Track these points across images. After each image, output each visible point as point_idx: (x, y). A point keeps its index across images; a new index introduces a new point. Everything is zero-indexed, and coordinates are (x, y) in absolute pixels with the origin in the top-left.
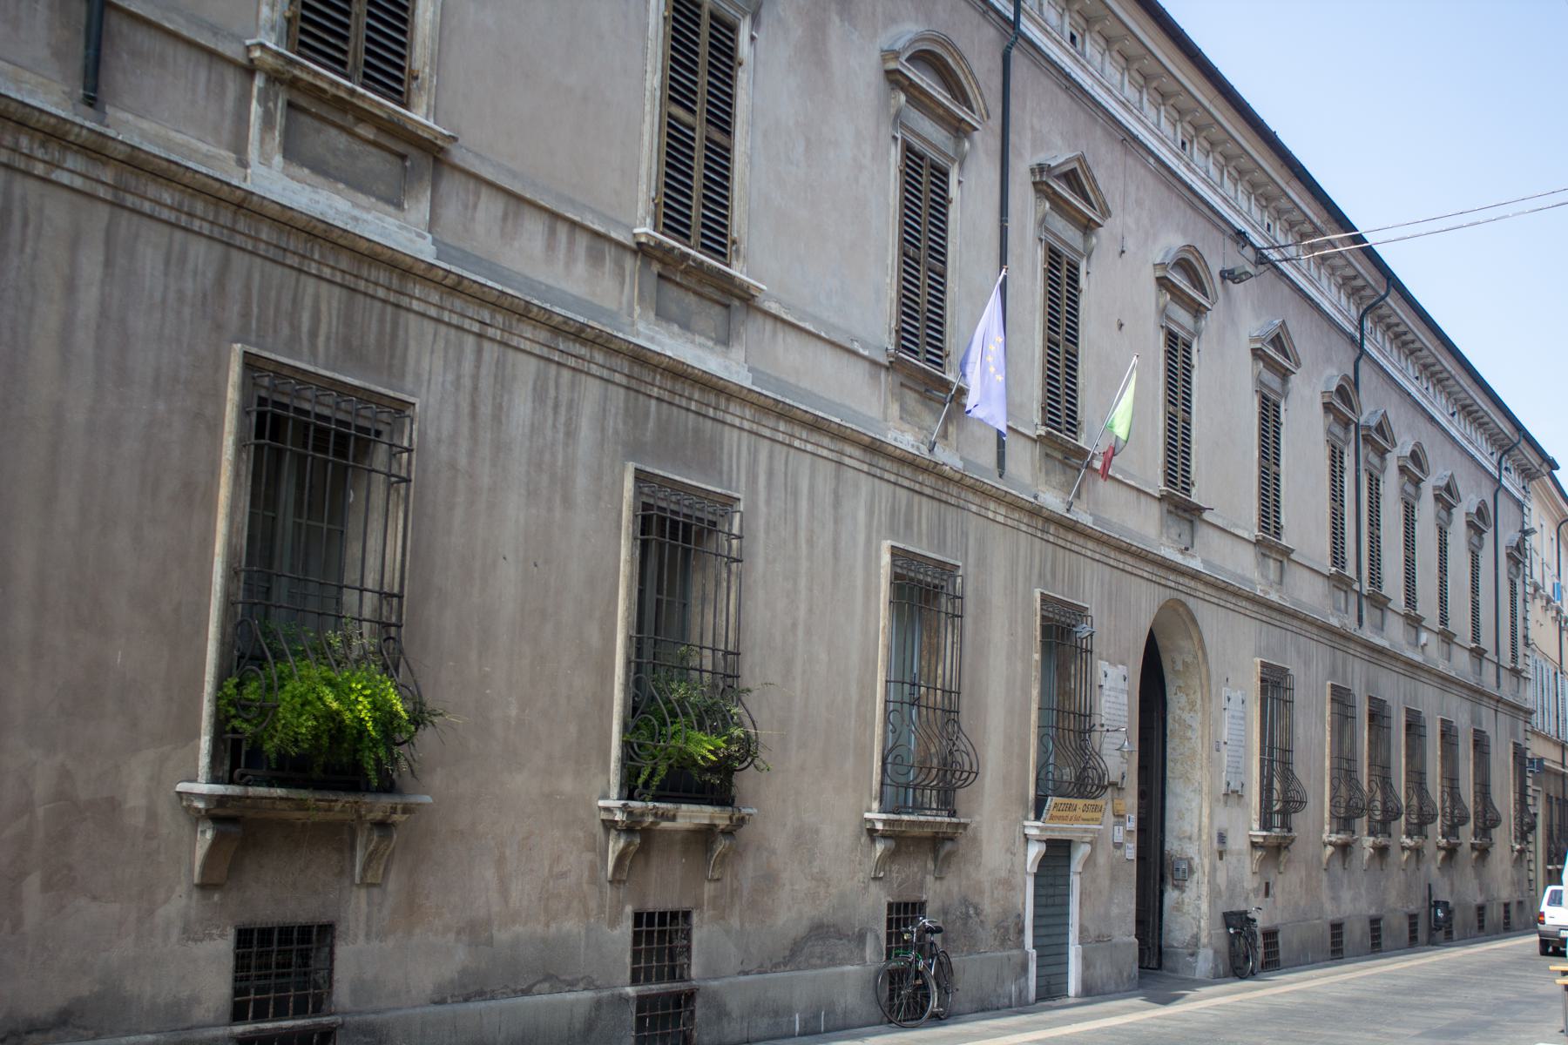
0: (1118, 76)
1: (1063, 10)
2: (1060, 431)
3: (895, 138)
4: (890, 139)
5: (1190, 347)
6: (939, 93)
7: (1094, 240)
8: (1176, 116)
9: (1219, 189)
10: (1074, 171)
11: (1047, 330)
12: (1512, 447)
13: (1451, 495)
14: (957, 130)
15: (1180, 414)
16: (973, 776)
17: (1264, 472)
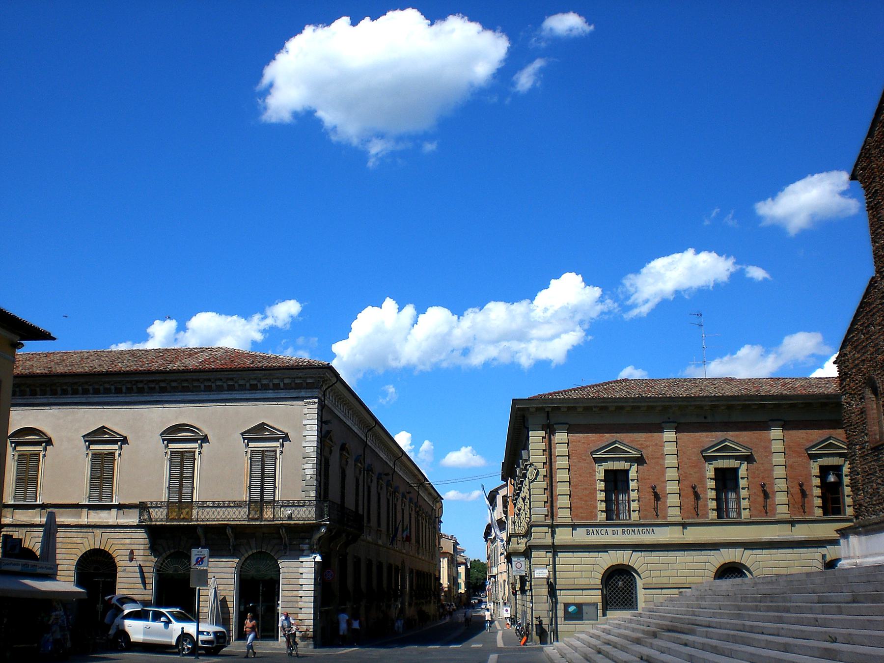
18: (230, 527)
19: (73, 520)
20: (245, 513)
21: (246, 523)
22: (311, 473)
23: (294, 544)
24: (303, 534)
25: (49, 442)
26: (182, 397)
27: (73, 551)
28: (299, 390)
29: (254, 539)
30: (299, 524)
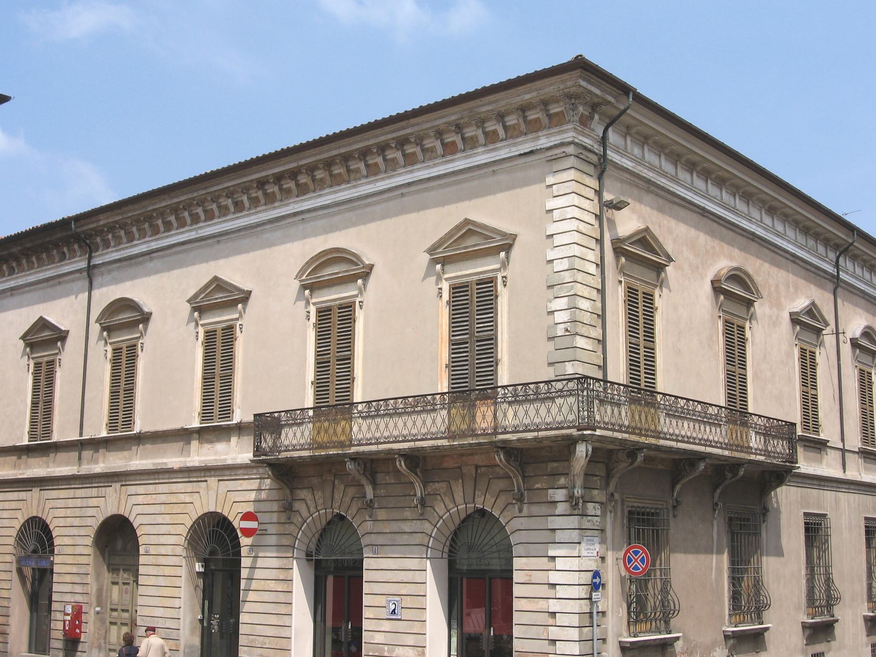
0: (732, 199)
1: (660, 152)
2: (810, 433)
3: (620, 282)
4: (717, 317)
5: (743, 328)
6: (642, 252)
7: (663, 274)
8: (734, 190)
9: (826, 259)
10: (644, 238)
11: (802, 387)
12: (848, 247)
13: (652, 250)
14: (658, 268)
15: (869, 408)
16: (839, 600)
17: (805, 396)
18: (403, 455)
19: (68, 468)
20: (571, 409)
21: (445, 442)
22: (566, 320)
23: (538, 489)
24: (555, 464)
25: (146, 318)
26: (333, 196)
27: (91, 512)
28: (534, 135)
29: (460, 481)
30: (527, 440)
